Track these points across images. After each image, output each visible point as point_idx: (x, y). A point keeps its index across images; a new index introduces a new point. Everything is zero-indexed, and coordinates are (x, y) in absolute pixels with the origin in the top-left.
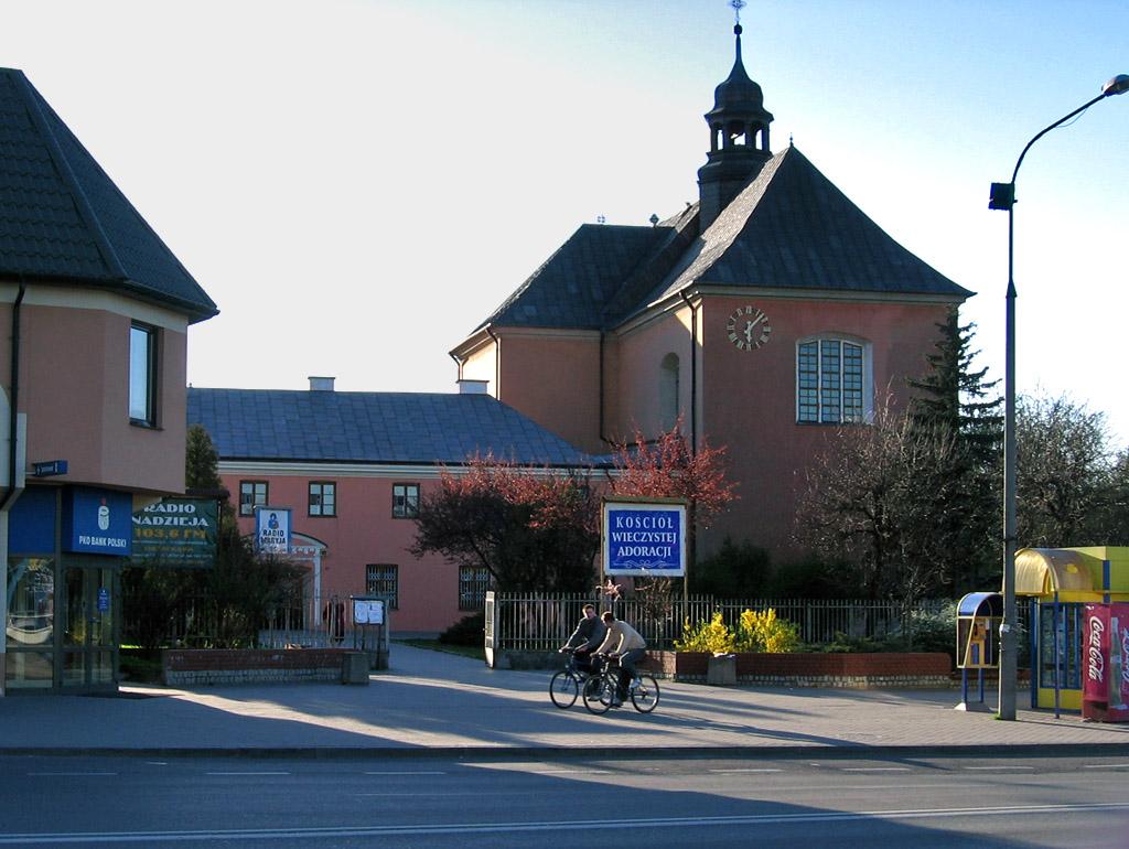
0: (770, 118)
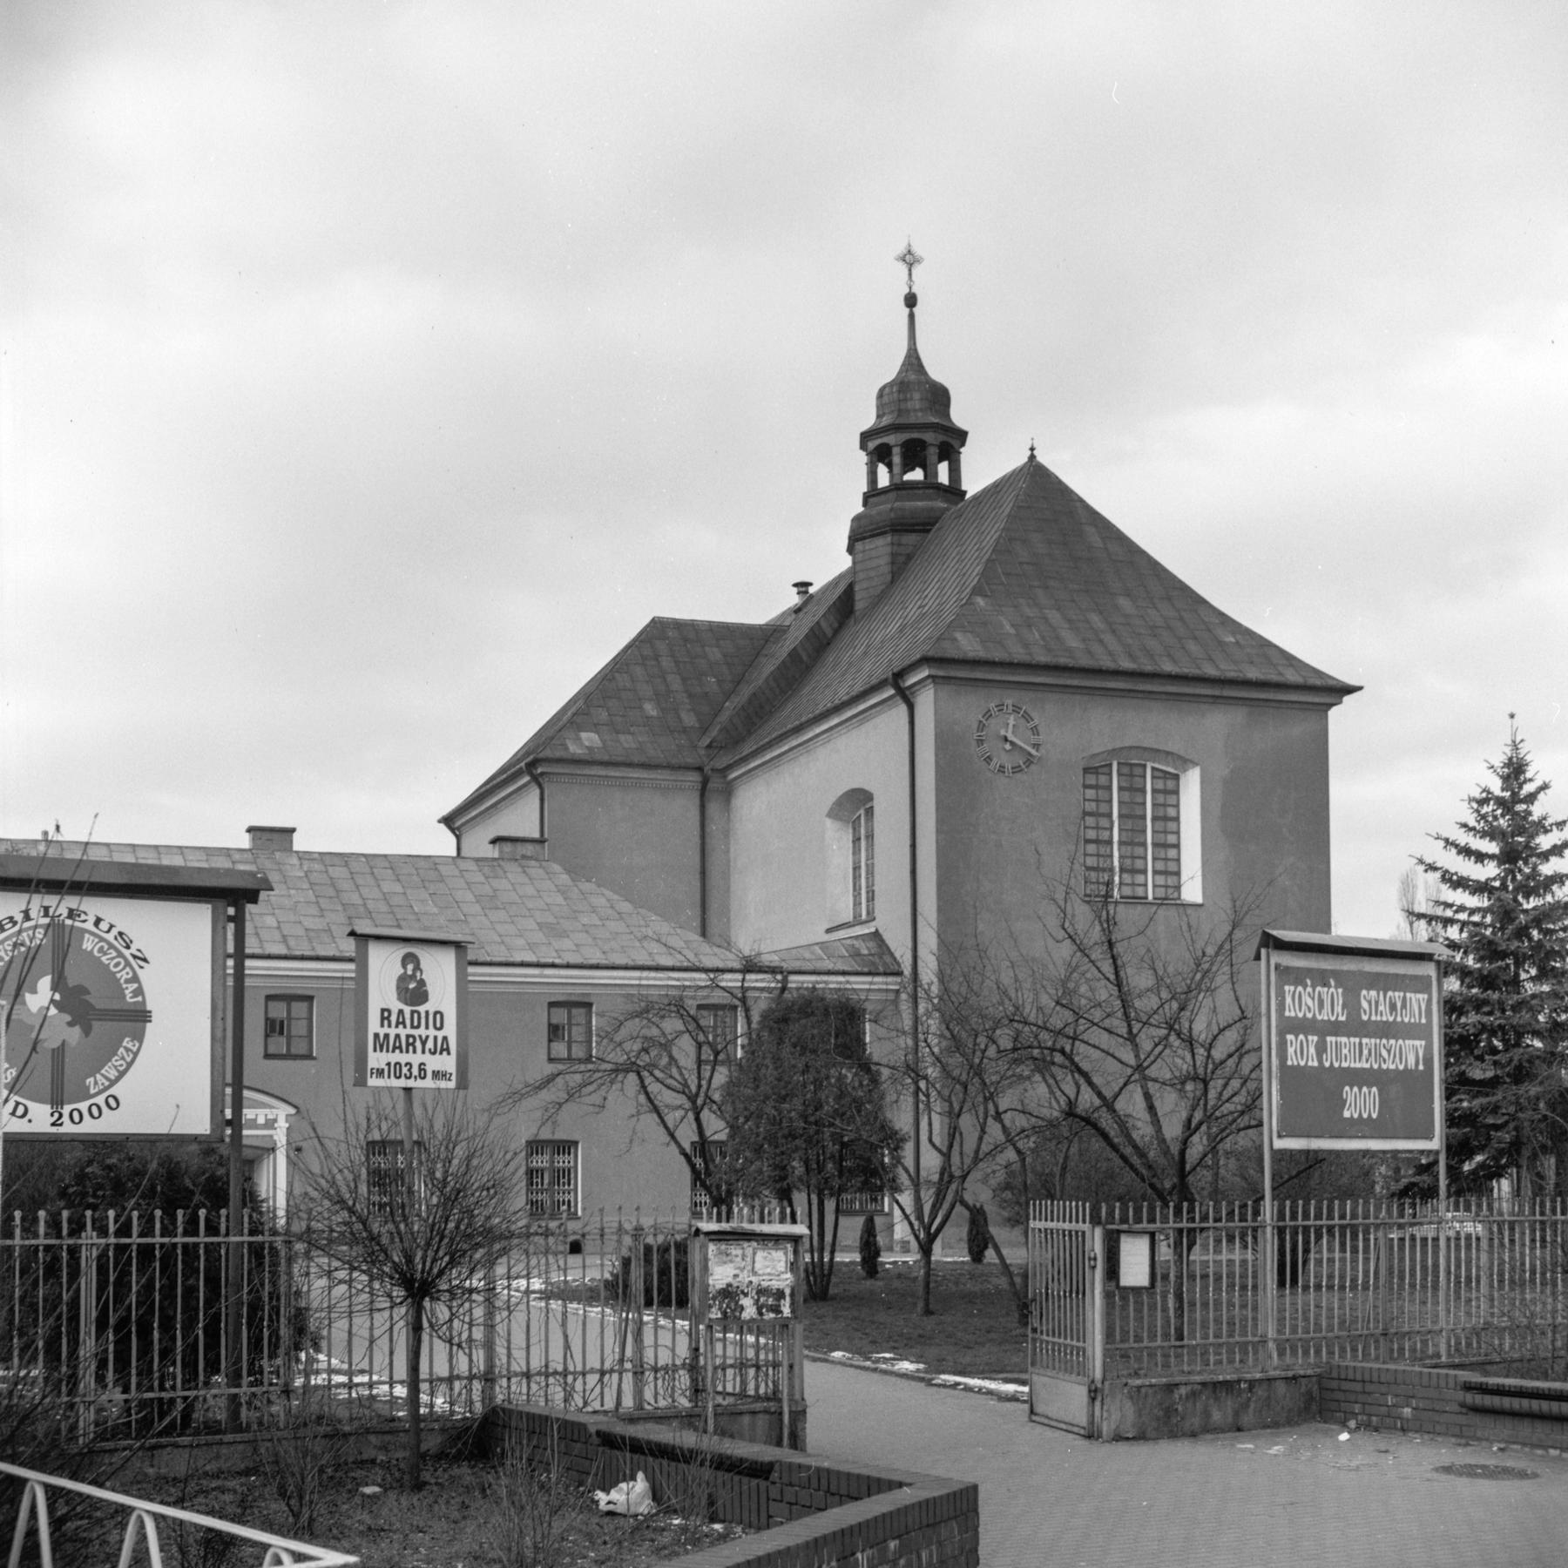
0: (962, 436)
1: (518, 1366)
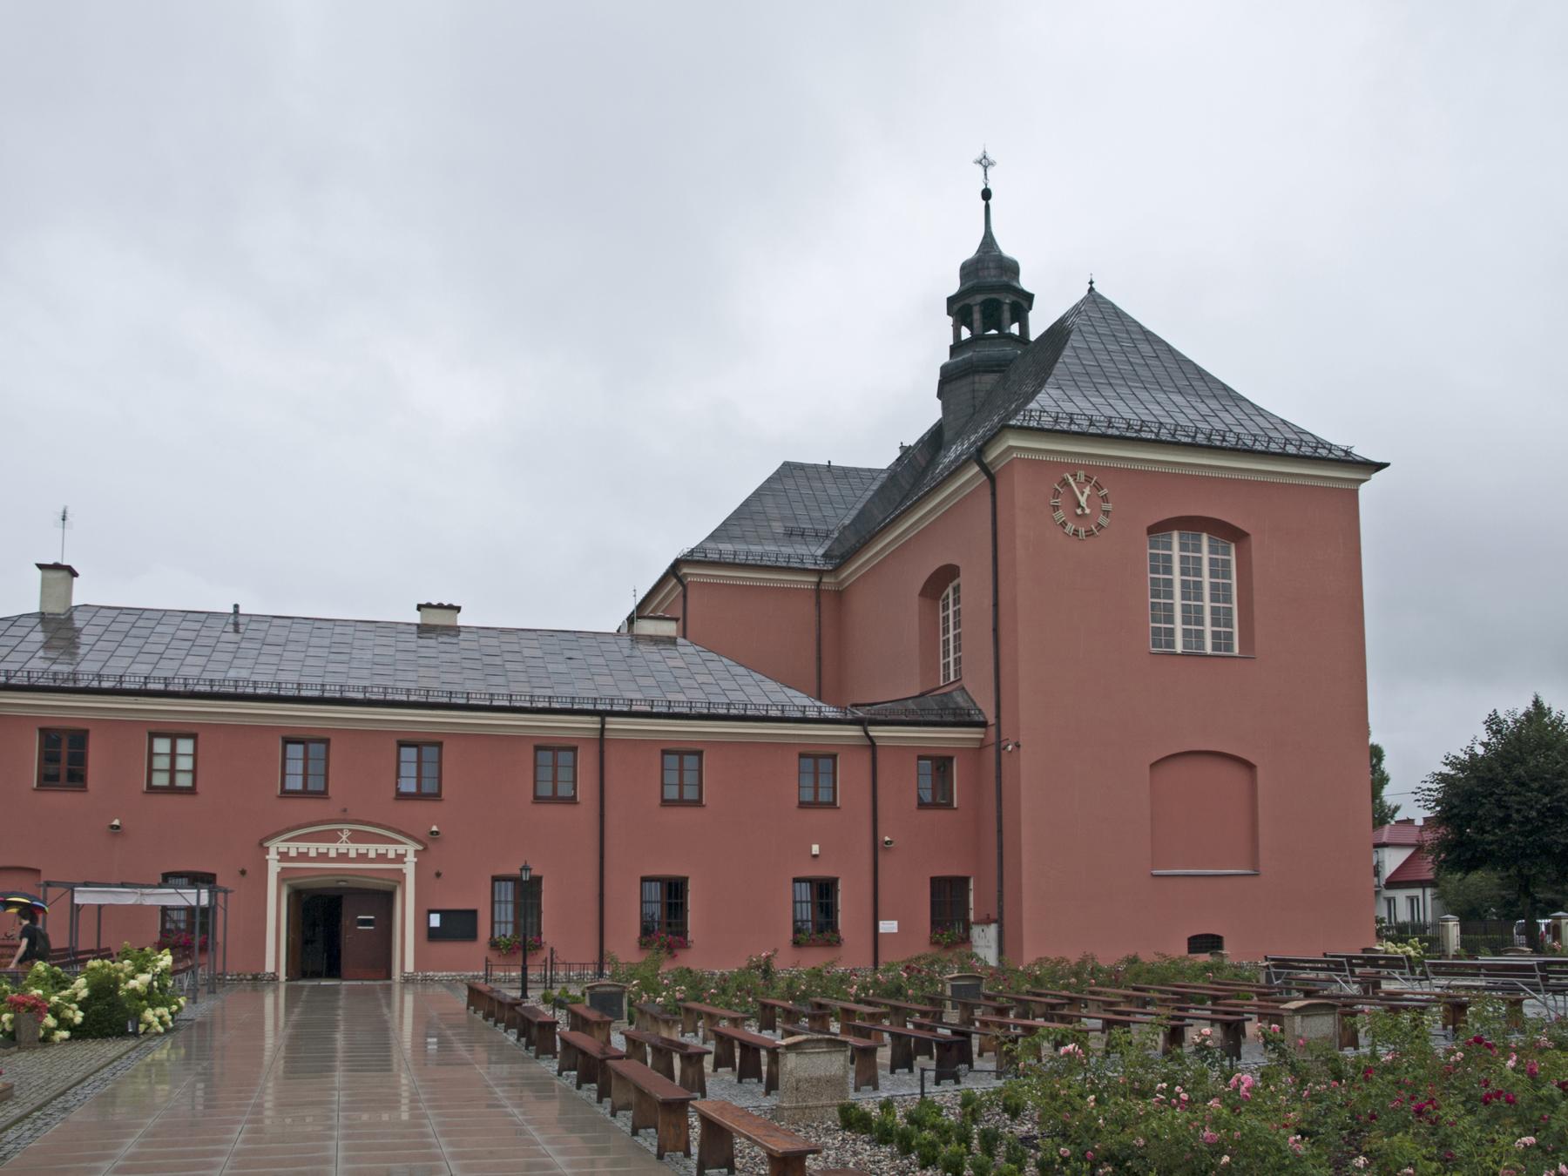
1: (804, 905)
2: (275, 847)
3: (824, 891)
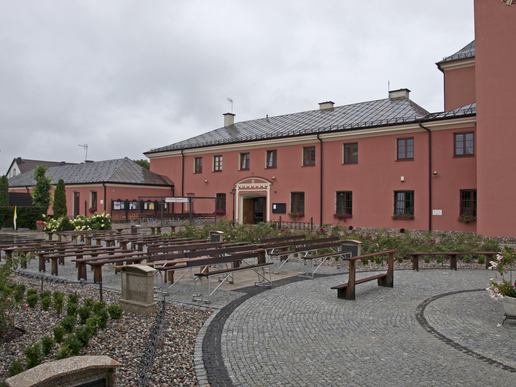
1: (401, 202)
2: (238, 185)
3: (409, 195)
